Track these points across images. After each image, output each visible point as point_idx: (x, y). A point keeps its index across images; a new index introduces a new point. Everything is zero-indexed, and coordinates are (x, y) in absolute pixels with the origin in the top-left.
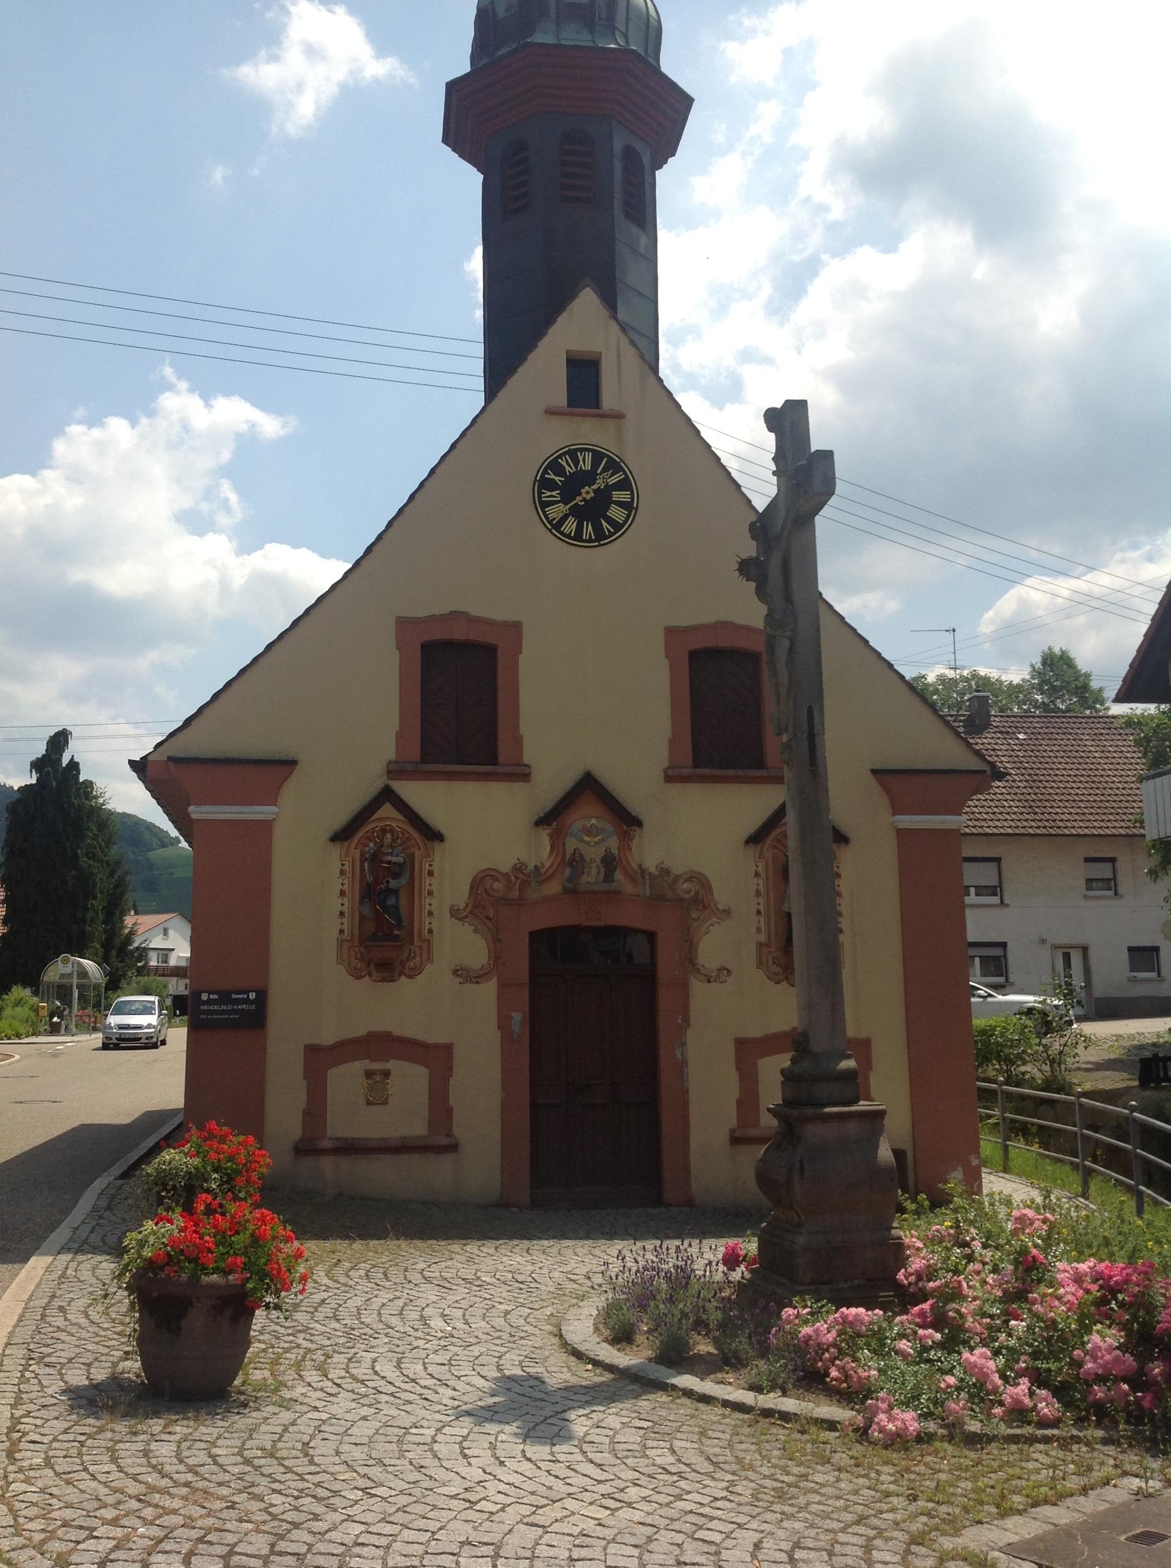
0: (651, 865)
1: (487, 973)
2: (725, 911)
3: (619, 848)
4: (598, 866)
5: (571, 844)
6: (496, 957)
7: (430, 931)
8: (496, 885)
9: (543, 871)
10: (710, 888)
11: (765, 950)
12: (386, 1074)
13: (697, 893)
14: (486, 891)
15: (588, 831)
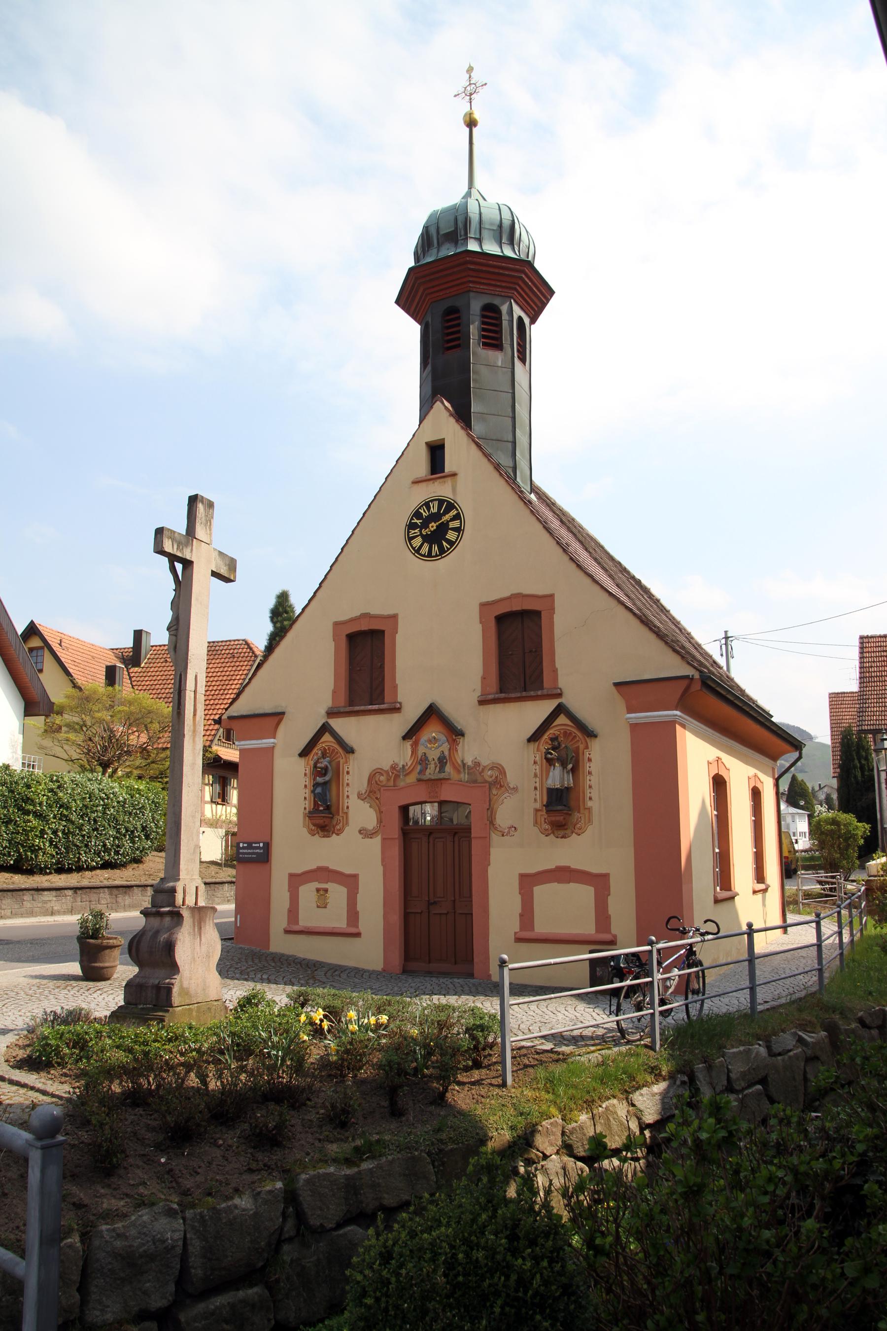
0: (469, 761)
1: (376, 832)
2: (514, 788)
3: (450, 749)
4: (435, 763)
5: (421, 750)
6: (380, 821)
7: (348, 807)
8: (382, 778)
9: (407, 768)
10: (505, 773)
11: (539, 813)
12: (326, 890)
13: (497, 777)
14: (376, 782)
15: (430, 741)
